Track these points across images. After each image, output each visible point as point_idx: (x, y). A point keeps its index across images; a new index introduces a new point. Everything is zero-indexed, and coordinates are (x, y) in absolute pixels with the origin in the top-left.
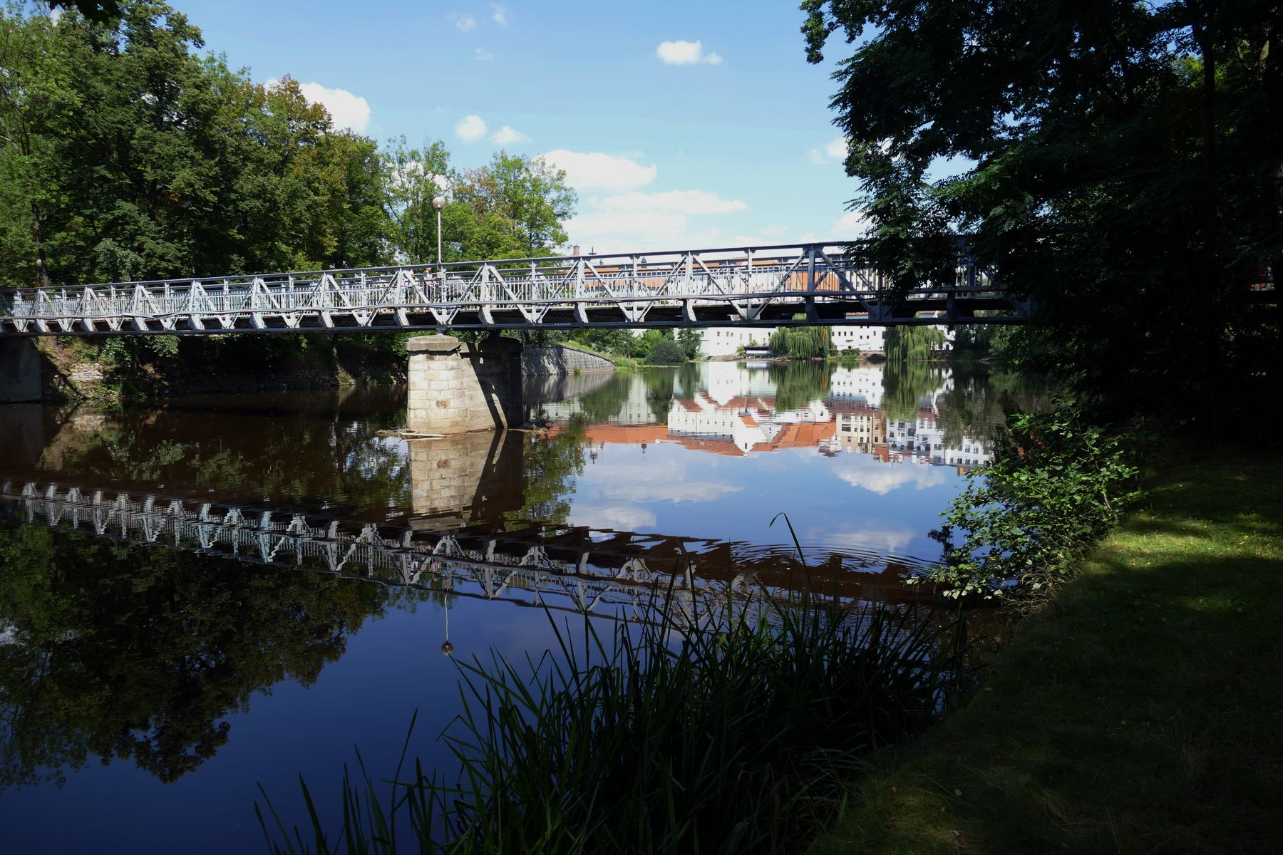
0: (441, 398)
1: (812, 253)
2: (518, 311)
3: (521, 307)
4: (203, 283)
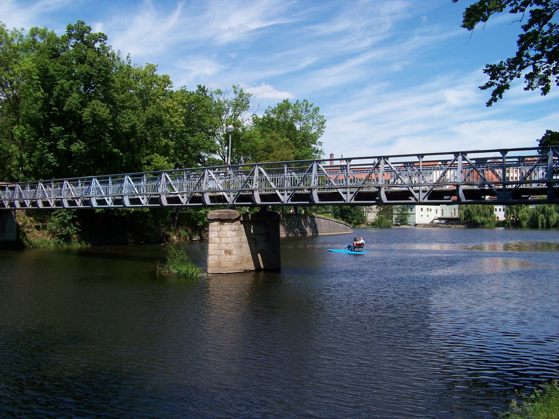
0: (228, 248)
1: (460, 157)
2: (276, 194)
3: (278, 192)
4: (131, 176)
